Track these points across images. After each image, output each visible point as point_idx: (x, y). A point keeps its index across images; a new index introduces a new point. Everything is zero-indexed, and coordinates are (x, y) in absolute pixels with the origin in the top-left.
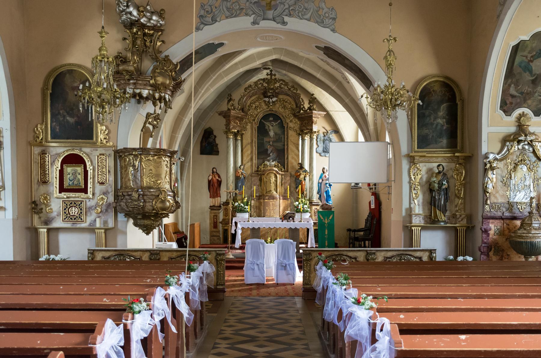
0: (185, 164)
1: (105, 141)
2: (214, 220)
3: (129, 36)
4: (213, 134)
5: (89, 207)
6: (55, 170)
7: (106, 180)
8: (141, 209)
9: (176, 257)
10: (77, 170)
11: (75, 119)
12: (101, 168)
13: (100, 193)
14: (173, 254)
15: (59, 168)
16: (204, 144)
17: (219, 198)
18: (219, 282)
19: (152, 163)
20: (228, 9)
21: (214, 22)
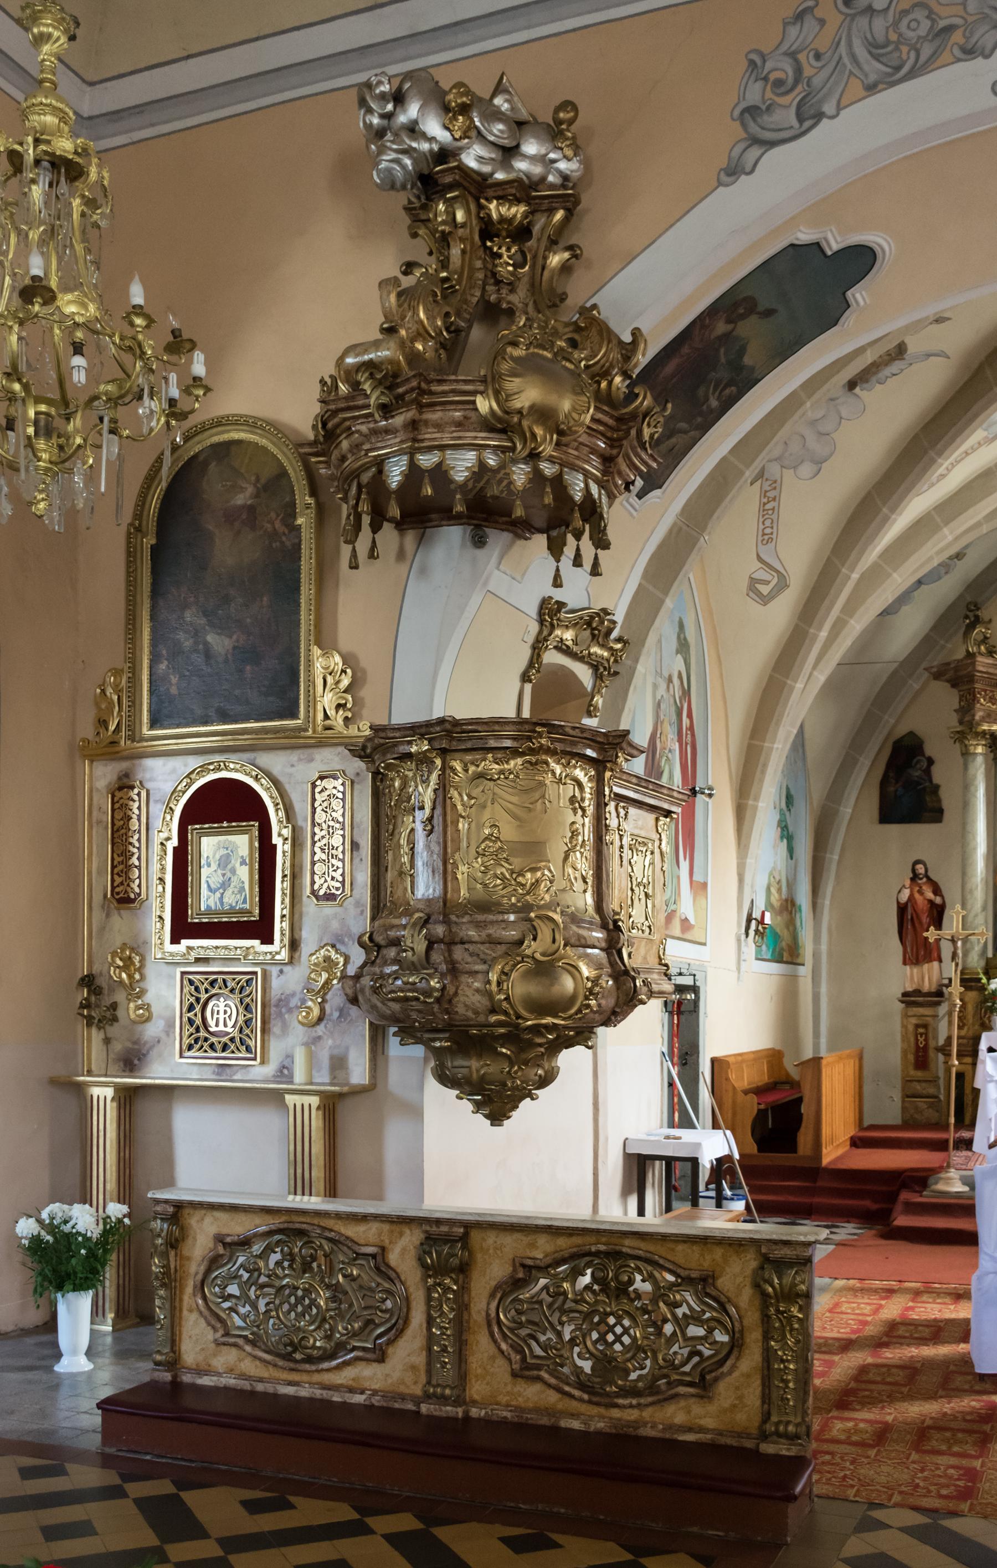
0: (828, 855)
1: (338, 720)
2: (917, 1040)
3: (431, 253)
4: (923, 754)
5: (280, 1000)
6: (156, 848)
7: (343, 883)
8: (436, 1007)
9: (548, 1260)
10: (237, 847)
11: (235, 637)
12: (324, 833)
13: (321, 940)
14: (533, 1245)
15: (175, 842)
16: (892, 789)
17: (936, 964)
18: (774, 1418)
19: (497, 790)
20: (875, 48)
21: (807, 124)
